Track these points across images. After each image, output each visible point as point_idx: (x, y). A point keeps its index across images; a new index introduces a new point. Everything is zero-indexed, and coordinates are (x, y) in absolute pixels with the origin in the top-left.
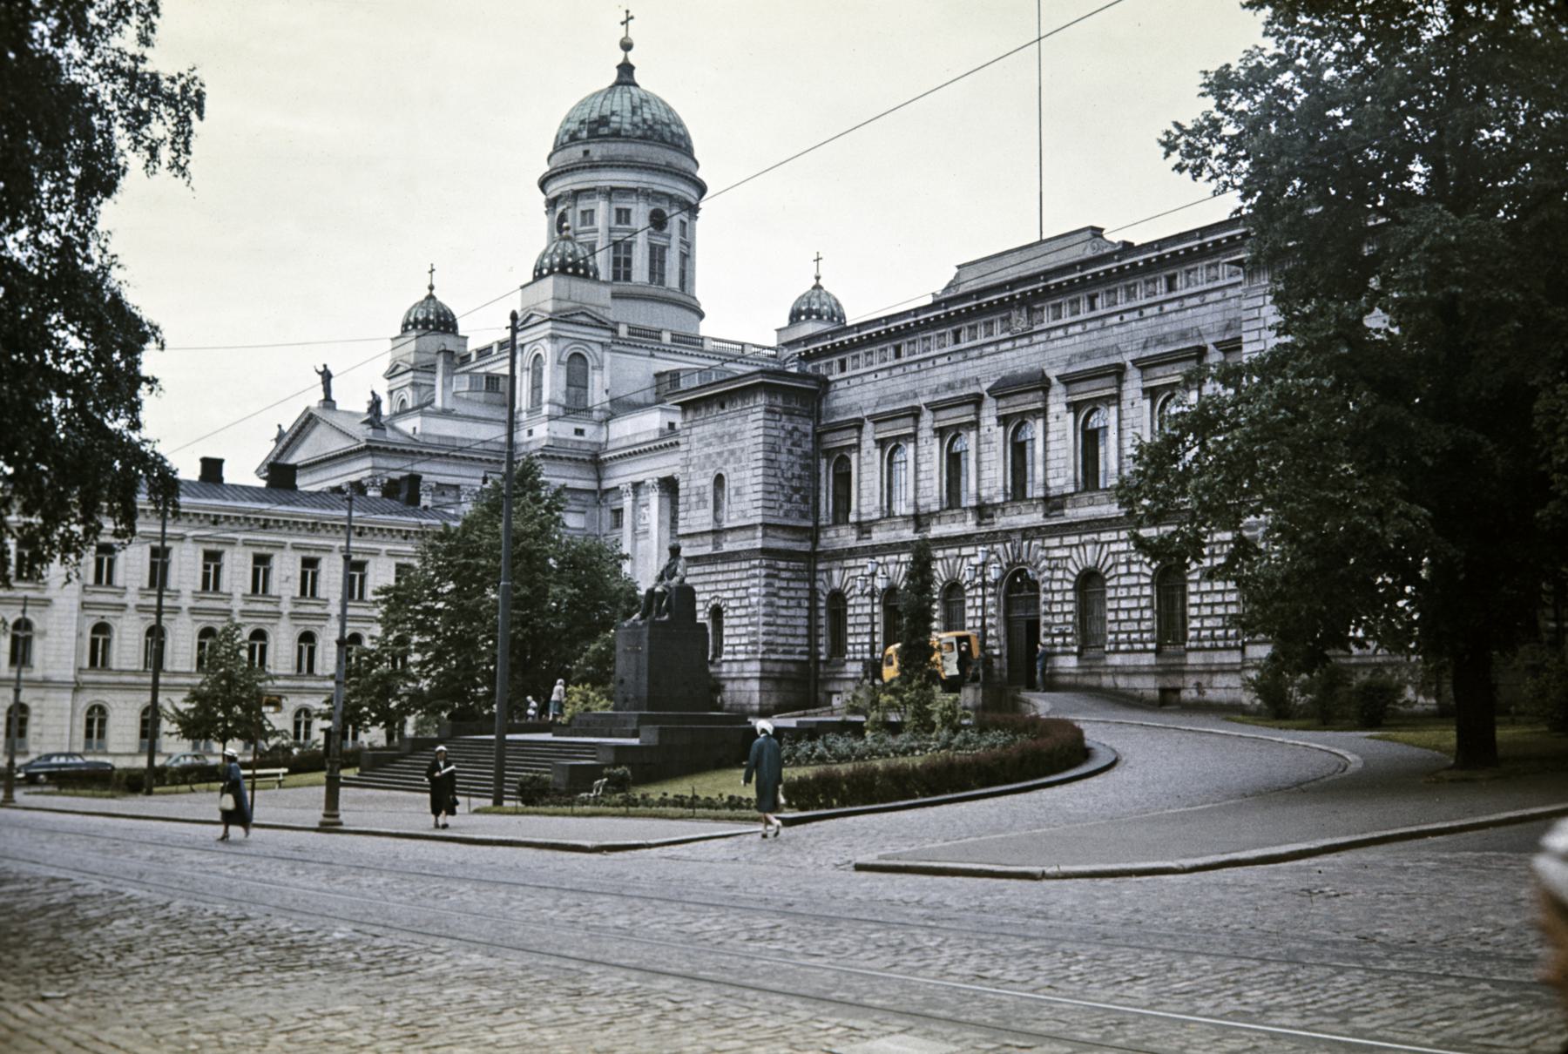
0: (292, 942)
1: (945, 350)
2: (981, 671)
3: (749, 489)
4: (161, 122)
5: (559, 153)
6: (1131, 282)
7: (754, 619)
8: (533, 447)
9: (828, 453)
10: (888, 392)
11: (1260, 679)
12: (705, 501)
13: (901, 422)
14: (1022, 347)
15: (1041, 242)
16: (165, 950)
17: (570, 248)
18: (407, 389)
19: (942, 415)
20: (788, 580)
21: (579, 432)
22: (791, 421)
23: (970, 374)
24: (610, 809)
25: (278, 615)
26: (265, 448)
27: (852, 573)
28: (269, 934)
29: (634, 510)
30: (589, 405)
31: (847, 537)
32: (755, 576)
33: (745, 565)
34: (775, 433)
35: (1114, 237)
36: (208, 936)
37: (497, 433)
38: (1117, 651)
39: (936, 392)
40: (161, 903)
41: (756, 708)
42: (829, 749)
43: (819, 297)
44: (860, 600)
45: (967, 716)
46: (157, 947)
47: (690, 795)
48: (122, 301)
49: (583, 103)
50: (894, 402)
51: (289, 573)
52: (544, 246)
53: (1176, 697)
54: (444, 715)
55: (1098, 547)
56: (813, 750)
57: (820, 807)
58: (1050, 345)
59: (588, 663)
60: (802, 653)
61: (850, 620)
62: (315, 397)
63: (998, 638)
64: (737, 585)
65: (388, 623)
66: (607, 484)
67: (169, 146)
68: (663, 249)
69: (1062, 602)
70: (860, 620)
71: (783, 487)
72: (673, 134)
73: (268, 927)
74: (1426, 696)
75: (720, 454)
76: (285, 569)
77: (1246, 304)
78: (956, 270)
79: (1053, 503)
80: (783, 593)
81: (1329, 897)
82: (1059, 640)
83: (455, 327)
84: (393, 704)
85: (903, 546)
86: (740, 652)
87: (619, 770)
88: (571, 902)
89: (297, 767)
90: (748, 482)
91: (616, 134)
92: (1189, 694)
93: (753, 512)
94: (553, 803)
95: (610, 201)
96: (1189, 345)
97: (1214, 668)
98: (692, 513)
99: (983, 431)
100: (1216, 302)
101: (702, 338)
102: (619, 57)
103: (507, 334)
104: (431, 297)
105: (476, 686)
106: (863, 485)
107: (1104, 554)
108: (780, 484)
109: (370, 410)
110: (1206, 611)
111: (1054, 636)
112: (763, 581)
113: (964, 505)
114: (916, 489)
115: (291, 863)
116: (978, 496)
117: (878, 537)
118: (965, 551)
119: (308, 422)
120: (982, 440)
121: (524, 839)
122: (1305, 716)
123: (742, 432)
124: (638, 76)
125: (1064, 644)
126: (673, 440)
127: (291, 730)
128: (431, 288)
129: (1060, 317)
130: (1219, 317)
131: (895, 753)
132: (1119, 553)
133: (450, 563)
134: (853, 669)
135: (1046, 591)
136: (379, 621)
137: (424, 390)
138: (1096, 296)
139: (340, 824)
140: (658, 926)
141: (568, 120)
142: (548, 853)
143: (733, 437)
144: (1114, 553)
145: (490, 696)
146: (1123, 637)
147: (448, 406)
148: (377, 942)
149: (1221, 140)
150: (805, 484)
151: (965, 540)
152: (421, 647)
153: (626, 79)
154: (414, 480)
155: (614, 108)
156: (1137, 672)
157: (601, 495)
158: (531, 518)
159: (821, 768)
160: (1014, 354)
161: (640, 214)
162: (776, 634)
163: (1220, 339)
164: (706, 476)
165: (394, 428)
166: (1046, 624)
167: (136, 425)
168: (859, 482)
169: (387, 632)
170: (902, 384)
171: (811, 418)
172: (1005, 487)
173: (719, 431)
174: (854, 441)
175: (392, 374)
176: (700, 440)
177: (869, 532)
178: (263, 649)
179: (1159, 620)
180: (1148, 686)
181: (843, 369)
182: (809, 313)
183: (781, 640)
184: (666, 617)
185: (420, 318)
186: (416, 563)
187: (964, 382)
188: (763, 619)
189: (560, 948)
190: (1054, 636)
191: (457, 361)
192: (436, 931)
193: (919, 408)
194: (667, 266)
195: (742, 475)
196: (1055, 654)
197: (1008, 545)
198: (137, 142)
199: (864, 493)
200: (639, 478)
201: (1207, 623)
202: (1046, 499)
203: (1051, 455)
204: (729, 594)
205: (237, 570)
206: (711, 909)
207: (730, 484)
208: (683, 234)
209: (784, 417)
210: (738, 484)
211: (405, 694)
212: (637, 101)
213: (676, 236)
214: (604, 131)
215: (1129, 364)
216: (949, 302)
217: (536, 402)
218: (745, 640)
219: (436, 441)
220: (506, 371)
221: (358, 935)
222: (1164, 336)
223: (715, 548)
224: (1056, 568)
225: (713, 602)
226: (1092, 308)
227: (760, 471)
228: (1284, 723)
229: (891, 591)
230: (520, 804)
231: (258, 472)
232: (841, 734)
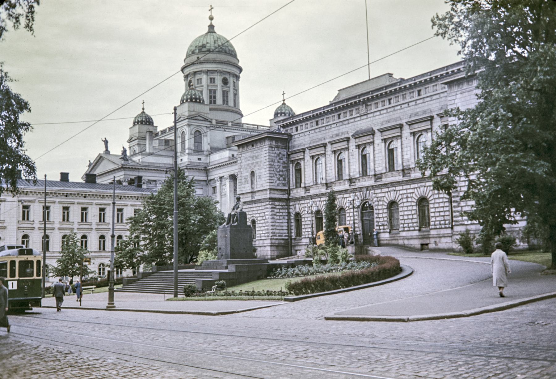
0: (89, 365)
1: (335, 122)
2: (354, 240)
3: (264, 176)
4: (21, 7)
6: (404, 93)
7: (267, 224)
8: (183, 165)
9: (292, 162)
10: (314, 138)
11: (461, 239)
12: (248, 181)
15: (370, 80)
16: (31, 371)
17: (193, 92)
18: (136, 146)
19: (335, 146)
20: (280, 209)
21: (199, 159)
23: (344, 130)
24: (220, 297)
25: (91, 229)
26: (85, 169)
27: (303, 205)
28: (79, 361)
29: (220, 187)
30: (203, 149)
31: (300, 192)
32: (267, 208)
33: (263, 204)
35: (397, 76)
36: (52, 363)
37: (169, 161)
38: (404, 231)
39: (332, 137)
40: (35, 346)
41: (269, 257)
42: (300, 271)
43: (284, 107)
44: (307, 216)
45: (351, 257)
46: (28, 369)
47: (251, 291)
48: (10, 92)
49: (196, 40)
50: (316, 142)
51: (95, 214)
52: (184, 92)
53: (426, 247)
54: (154, 264)
55: (426, 188)
56: (294, 272)
57: (303, 293)
58: (374, 118)
59: (206, 242)
60: (285, 236)
61: (303, 223)
62: (102, 150)
63: (359, 227)
64: (261, 211)
65: (132, 231)
66: (210, 178)
67: (25, 18)
68: (227, 92)
70: (307, 223)
71: (276, 175)
72: (229, 50)
73: (79, 358)
74: (524, 242)
75: (252, 164)
76: (93, 213)
77: (449, 99)
79: (377, 177)
80: (278, 214)
81: (542, 325)
82: (382, 227)
83: (153, 123)
84: (135, 260)
85: (323, 195)
86: (263, 236)
87: (221, 282)
88: (212, 340)
89: (99, 285)
90: (263, 173)
91: (209, 51)
92: (432, 246)
93: (266, 185)
94: (197, 295)
95: (207, 75)
96: (427, 115)
97: (441, 236)
98: (243, 186)
99: (350, 151)
100: (437, 99)
101: (243, 124)
102: (208, 22)
103: (173, 124)
104: (143, 112)
105: (165, 253)
106: (306, 173)
107: (398, 195)
109: (122, 154)
110: (437, 214)
111: (380, 226)
112: (270, 210)
113: (344, 179)
114: (326, 173)
115: (93, 325)
116: (350, 176)
117: (312, 192)
118: (345, 196)
119: (100, 159)
120: (350, 154)
121: (187, 311)
122: (477, 252)
123: (260, 155)
124: (216, 29)
125: (384, 229)
126: (234, 161)
127: (97, 271)
128: (143, 109)
129: (378, 107)
130: (438, 105)
131: (325, 271)
132: (403, 194)
133: (154, 208)
134: (305, 241)
135: (376, 209)
136: (128, 230)
137: (142, 146)
138: (391, 99)
139: (115, 307)
140: (253, 351)
141: (191, 46)
142: (197, 316)
145: (171, 257)
146: (437, 223)
147: (151, 151)
148: (127, 364)
149: (453, 23)
150: (284, 173)
151: (346, 191)
152: (144, 239)
153: (211, 30)
154: (140, 178)
156: (412, 238)
157: (208, 182)
158: (183, 190)
159: (303, 278)
160: (361, 122)
161: (219, 80)
162: (276, 229)
163: (439, 113)
164: (248, 172)
165: (131, 160)
166: (377, 222)
167: (20, 145)
168: (304, 172)
169: (132, 234)
170: (320, 135)
171: (286, 149)
172: (359, 171)
174: (302, 157)
175: (130, 141)
176: (245, 159)
177: (309, 190)
178: (86, 242)
179: (419, 218)
180: (416, 243)
181: (297, 130)
182: (281, 114)
183: (277, 231)
184: (236, 224)
185: (140, 120)
186: (142, 208)
187: (342, 133)
188: (271, 224)
189: (211, 365)
190: (380, 226)
191: (154, 135)
192: (154, 357)
193: (326, 144)
194: (229, 99)
195: (261, 171)
196: (380, 233)
197: (361, 193)
198: (10, 15)
199: (307, 176)
200: (222, 175)
201: (438, 219)
202: (375, 175)
203: (376, 159)
205: (75, 213)
206: (274, 342)
208: (234, 86)
209: (276, 149)
211: (139, 256)
212: (216, 38)
213: (232, 89)
214: (204, 49)
215: (405, 124)
216: (336, 104)
217: (183, 149)
218: (264, 232)
219: (147, 164)
220: (173, 138)
221: (119, 361)
222: (418, 113)
223: (252, 198)
224: (380, 200)
226: (390, 103)
227: (268, 169)
228: (470, 255)
229: (318, 212)
230: (184, 296)
231: (82, 178)
232: (304, 265)
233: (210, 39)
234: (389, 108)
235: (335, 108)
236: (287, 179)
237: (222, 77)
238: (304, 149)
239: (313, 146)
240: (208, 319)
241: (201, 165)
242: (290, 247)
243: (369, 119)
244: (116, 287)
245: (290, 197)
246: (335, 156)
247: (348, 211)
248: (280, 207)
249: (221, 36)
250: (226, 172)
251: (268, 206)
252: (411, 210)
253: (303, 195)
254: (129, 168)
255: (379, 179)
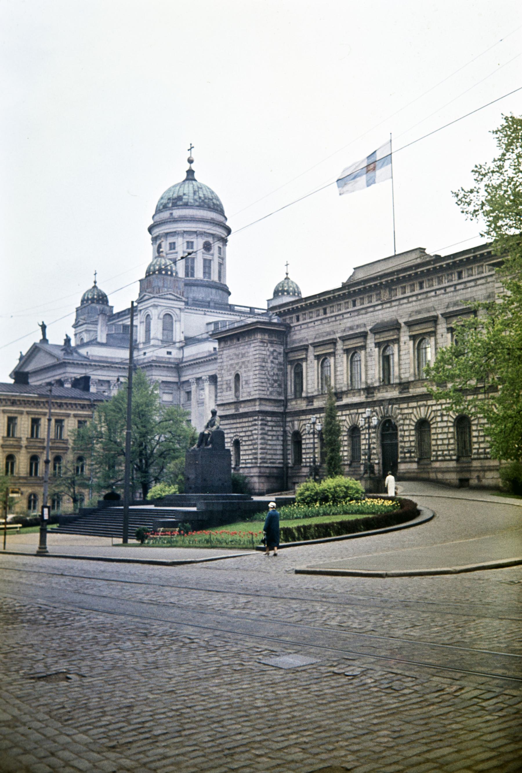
3: (252, 381)
5: (158, 215)
7: (256, 446)
9: (291, 362)
12: (230, 387)
13: (328, 346)
14: (386, 308)
15: (395, 256)
18: (84, 333)
19: (347, 343)
20: (272, 426)
21: (169, 353)
22: (272, 346)
27: (304, 422)
33: (251, 419)
34: (264, 352)
38: (437, 461)
39: (344, 331)
49: (169, 190)
55: (426, 408)
58: (400, 307)
61: (304, 446)
64: (247, 429)
66: (183, 379)
69: (409, 436)
71: (269, 380)
75: (237, 364)
78: (353, 270)
80: (270, 433)
82: (408, 455)
83: (107, 301)
90: (251, 378)
91: (186, 205)
92: (474, 482)
95: (183, 238)
97: (486, 468)
98: (224, 393)
99: (368, 350)
102: (187, 166)
104: (95, 287)
106: (309, 378)
107: (429, 411)
108: (267, 378)
109: (65, 344)
111: (405, 453)
118: (360, 411)
119: (35, 350)
123: (248, 353)
124: (196, 176)
128: (95, 282)
129: (414, 291)
130: (484, 292)
135: (401, 430)
137: (92, 333)
141: (162, 198)
143: (243, 355)
144: (434, 411)
150: (280, 378)
153: (190, 177)
155: (185, 192)
161: (199, 243)
162: (266, 453)
164: (231, 374)
168: (307, 376)
170: (327, 328)
173: (237, 352)
174: (304, 356)
179: (458, 444)
180: (453, 477)
185: (90, 297)
187: (358, 326)
190: (405, 453)
193: (336, 339)
197: (382, 407)
201: (482, 445)
203: (402, 362)
204: (242, 434)
207: (243, 379)
209: (269, 345)
210: (246, 379)
218: (251, 457)
222: (457, 302)
224: (406, 419)
225: (235, 438)
231: (10, 376)
233: (188, 189)
234: (420, 294)
235: (320, 301)
236: (283, 386)
237: (204, 241)
238: (307, 346)
239: (320, 342)
240: (158, 569)
241: (172, 361)
242: (285, 478)
243: (394, 308)
244: (49, 527)
245: (287, 411)
246: (347, 357)
247: (364, 432)
248: (272, 424)
249: (204, 185)
250: (205, 372)
251: (256, 422)
252: (447, 433)
253: (304, 408)
254: (73, 363)
255: (405, 389)
